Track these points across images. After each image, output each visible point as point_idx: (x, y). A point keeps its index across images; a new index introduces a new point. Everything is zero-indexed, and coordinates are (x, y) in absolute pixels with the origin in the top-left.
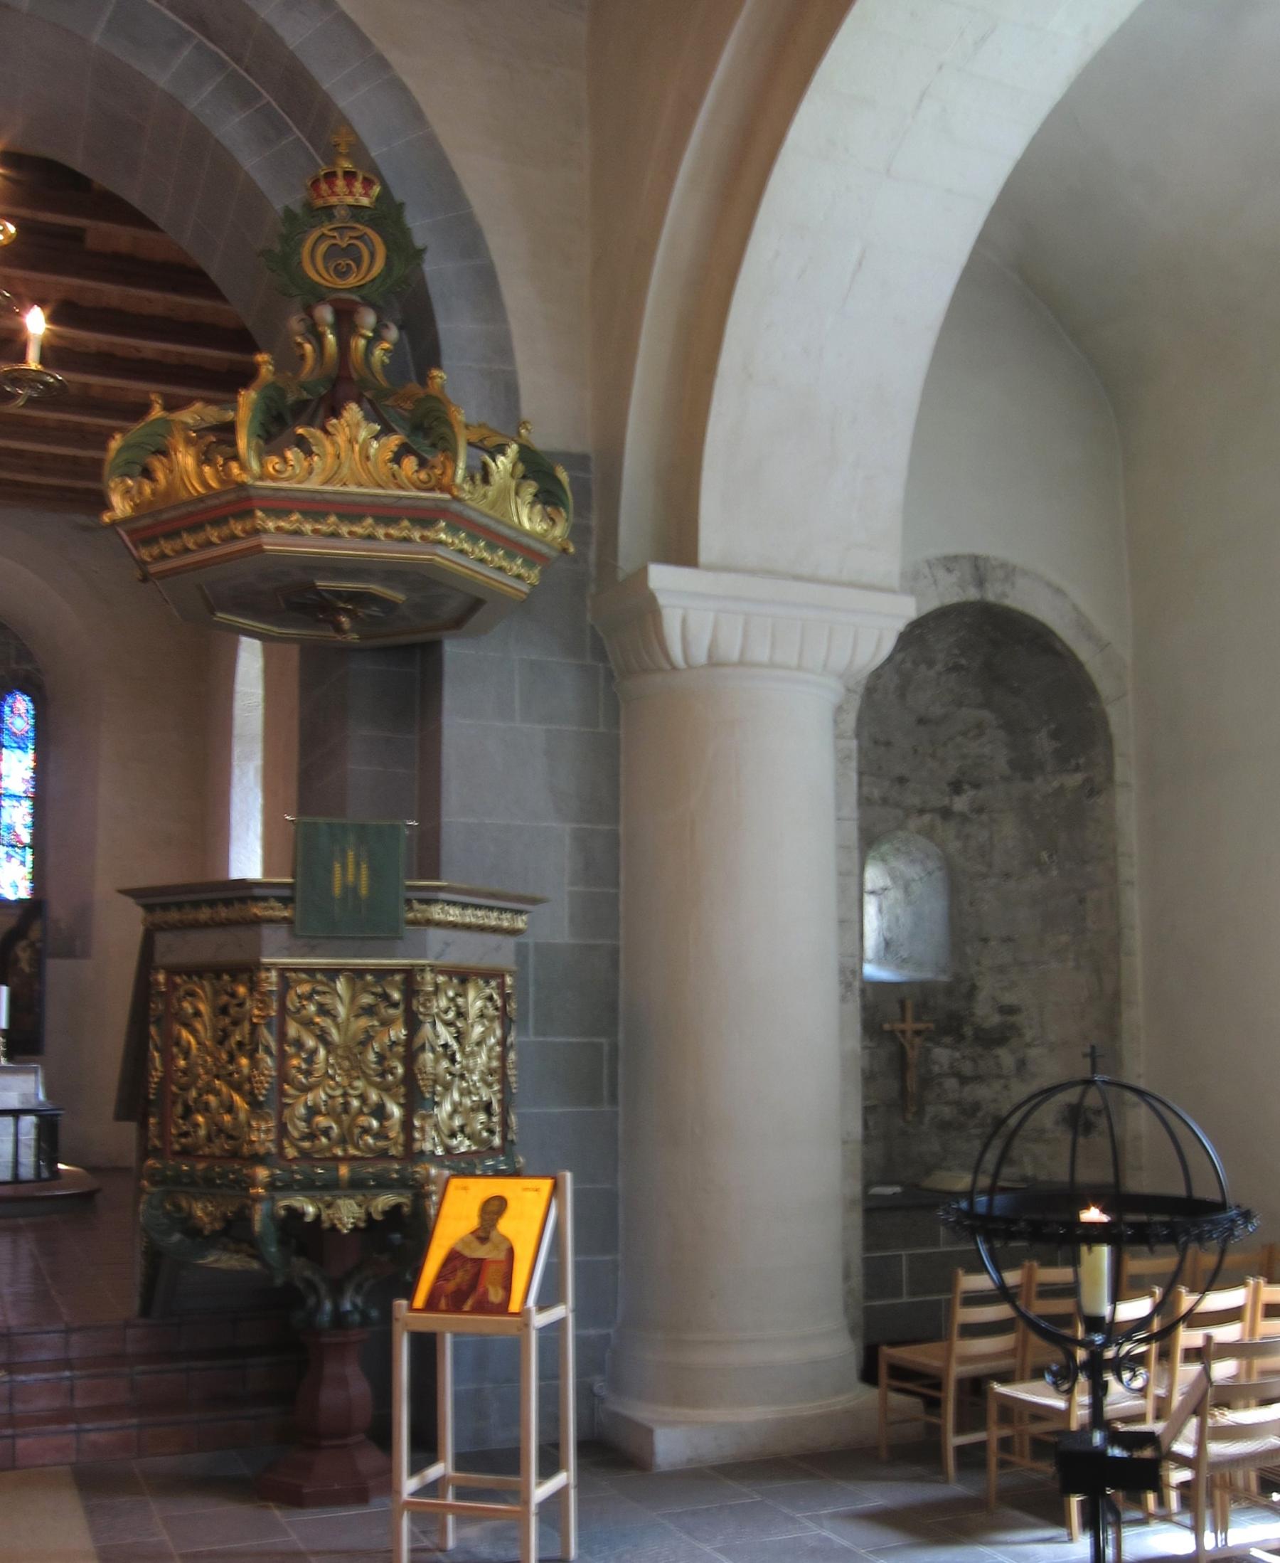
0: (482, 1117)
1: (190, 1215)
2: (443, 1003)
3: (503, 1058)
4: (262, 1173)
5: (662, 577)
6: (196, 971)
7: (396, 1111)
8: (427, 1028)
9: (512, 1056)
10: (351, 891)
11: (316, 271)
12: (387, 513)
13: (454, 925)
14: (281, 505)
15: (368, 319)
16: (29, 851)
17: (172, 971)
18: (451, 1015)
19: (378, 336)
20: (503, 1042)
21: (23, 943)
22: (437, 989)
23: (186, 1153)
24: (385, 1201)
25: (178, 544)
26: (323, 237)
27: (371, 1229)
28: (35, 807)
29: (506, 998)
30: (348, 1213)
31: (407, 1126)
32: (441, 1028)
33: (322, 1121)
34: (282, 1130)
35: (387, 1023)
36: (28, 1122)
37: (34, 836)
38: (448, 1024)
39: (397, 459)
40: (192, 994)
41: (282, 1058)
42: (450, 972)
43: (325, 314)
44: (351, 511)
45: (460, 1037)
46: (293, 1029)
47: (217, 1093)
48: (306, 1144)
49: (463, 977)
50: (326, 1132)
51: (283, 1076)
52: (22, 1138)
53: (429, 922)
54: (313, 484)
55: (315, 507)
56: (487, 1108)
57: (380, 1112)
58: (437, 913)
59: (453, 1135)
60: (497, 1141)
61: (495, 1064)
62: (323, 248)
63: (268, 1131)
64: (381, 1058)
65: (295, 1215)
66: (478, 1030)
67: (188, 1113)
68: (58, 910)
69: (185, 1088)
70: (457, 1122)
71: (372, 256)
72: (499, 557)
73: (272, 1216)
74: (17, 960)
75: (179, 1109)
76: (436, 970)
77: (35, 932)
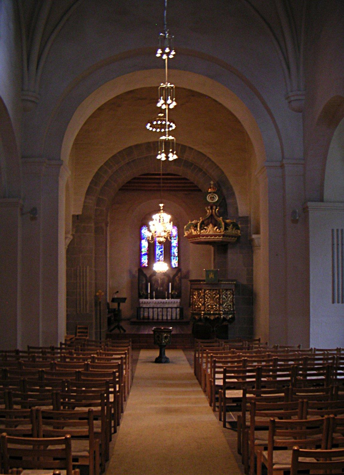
0: (230, 307)
1: (195, 318)
2: (224, 293)
3: (233, 299)
4: (203, 312)
5: (254, 236)
6: (196, 289)
7: (218, 306)
8: (221, 296)
9: (234, 299)
10: (212, 278)
11: (209, 200)
12: (215, 236)
13: (225, 284)
14: (203, 236)
15: (214, 207)
16: (177, 257)
17: (193, 289)
18: (225, 294)
19: (216, 208)
20: (233, 297)
21: (177, 277)
22: (223, 291)
23: (195, 310)
24: (217, 316)
25: (192, 239)
26: (209, 196)
27: (215, 319)
28: (178, 248)
29: (233, 292)
30: (212, 318)
31: (219, 307)
32: (224, 296)
33: (209, 306)
34: (205, 308)
35: (217, 295)
36: (178, 309)
37: (178, 254)
38: (225, 295)
39: (216, 229)
40: (195, 292)
41: (205, 299)
42: (225, 289)
43: (209, 207)
44: (211, 236)
45: (226, 297)
46: (206, 296)
47: (198, 303)
48: (208, 309)
49: (227, 290)
50: (210, 308)
51: (205, 301)
52: (177, 313)
53: (221, 284)
54: (207, 233)
55: (207, 236)
56: (230, 305)
57: (216, 306)
58: (222, 282)
59: (225, 308)
60: (232, 309)
61: (231, 300)
62: (210, 197)
63: (203, 308)
64: (216, 299)
65: (206, 317)
66: (229, 296)
67: (195, 306)
68: (184, 270)
69: (195, 303)
70: (226, 307)
71: (216, 197)
72: (228, 238)
73: (204, 317)
74: (176, 280)
75: (194, 305)
76: (223, 289)
77: (179, 275)
